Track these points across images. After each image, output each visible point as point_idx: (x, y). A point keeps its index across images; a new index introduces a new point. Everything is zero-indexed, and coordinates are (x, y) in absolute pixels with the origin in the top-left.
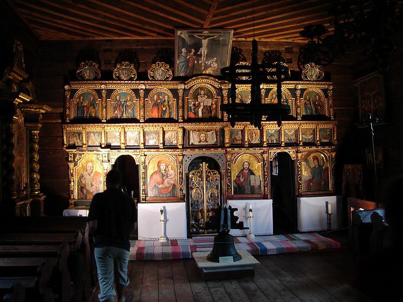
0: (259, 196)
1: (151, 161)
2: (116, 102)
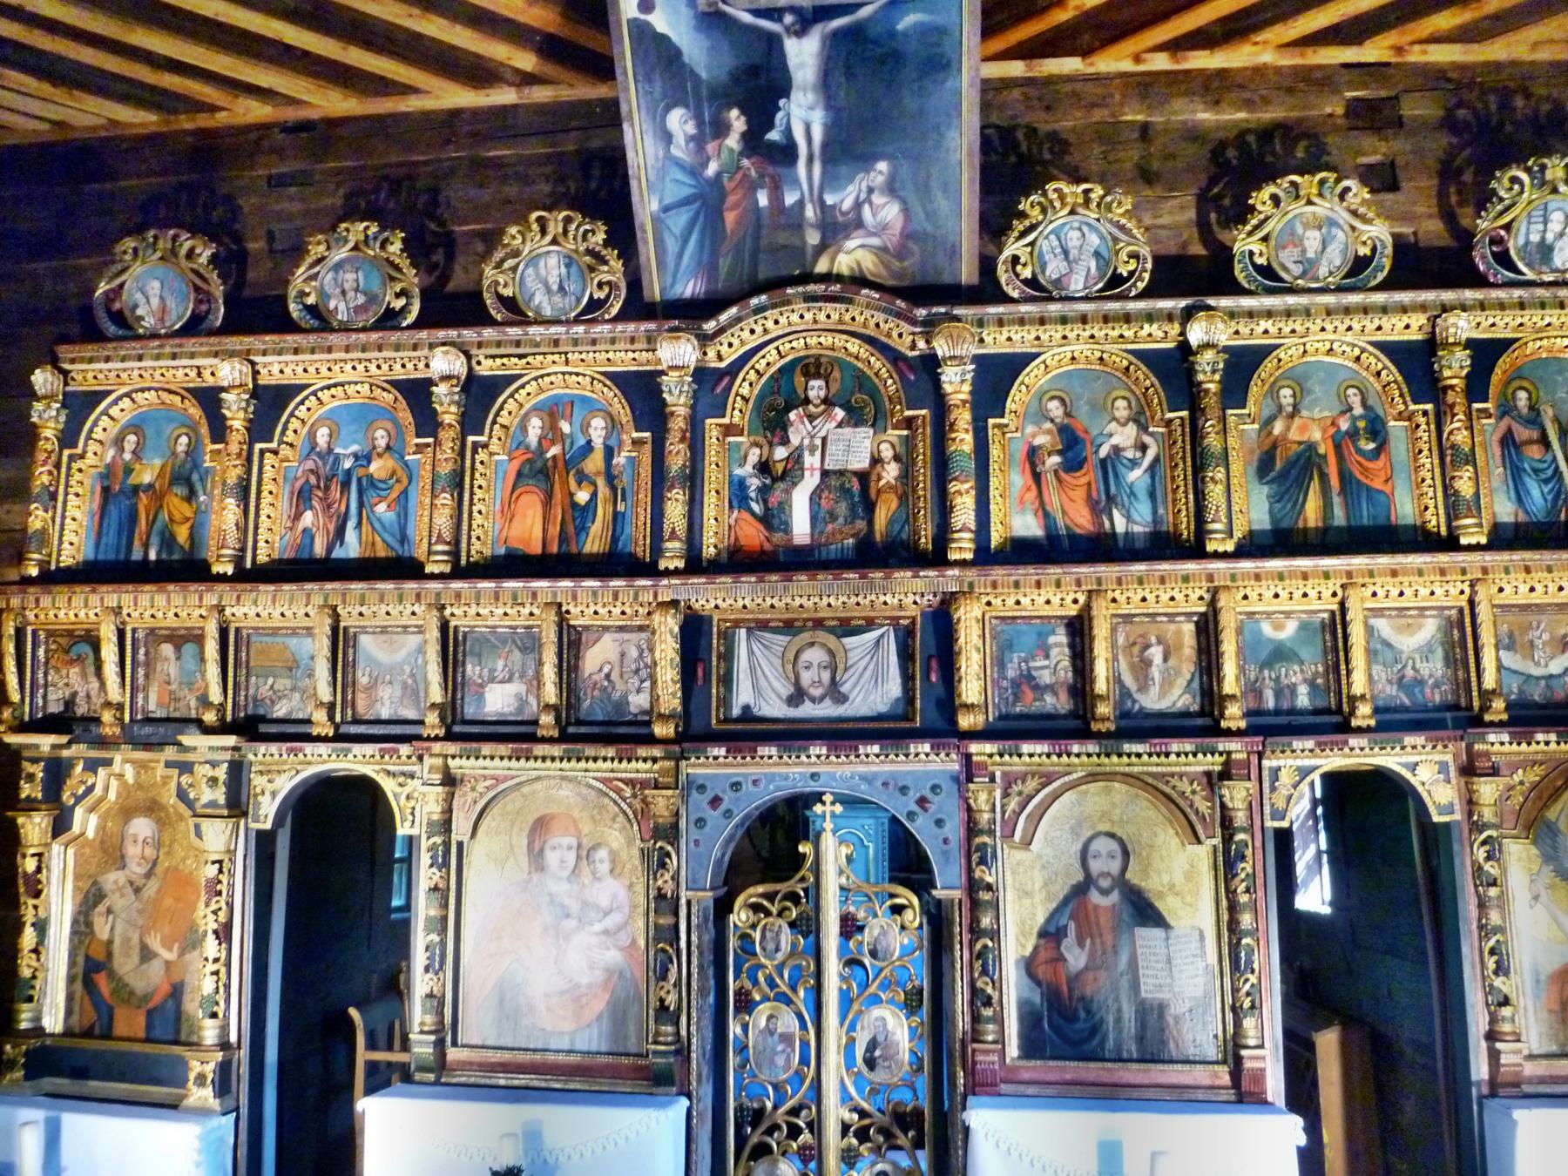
1: (495, 810)
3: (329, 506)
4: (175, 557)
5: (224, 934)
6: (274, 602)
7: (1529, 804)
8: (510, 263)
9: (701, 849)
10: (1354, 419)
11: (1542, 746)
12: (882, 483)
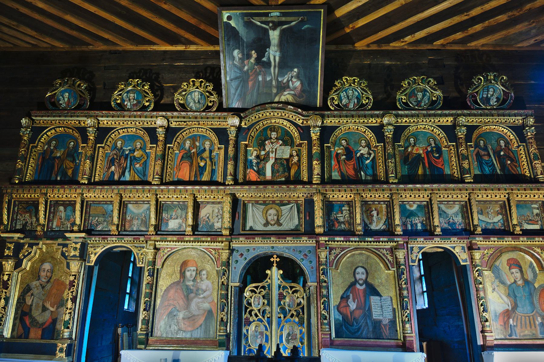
0: (393, 342)
1: (170, 259)
2: (114, 152)
3: (120, 165)
4: (67, 179)
5: (74, 300)
6: (101, 192)
7: (490, 260)
8: (184, 93)
9: (236, 270)
10: (432, 148)
11: (537, 243)
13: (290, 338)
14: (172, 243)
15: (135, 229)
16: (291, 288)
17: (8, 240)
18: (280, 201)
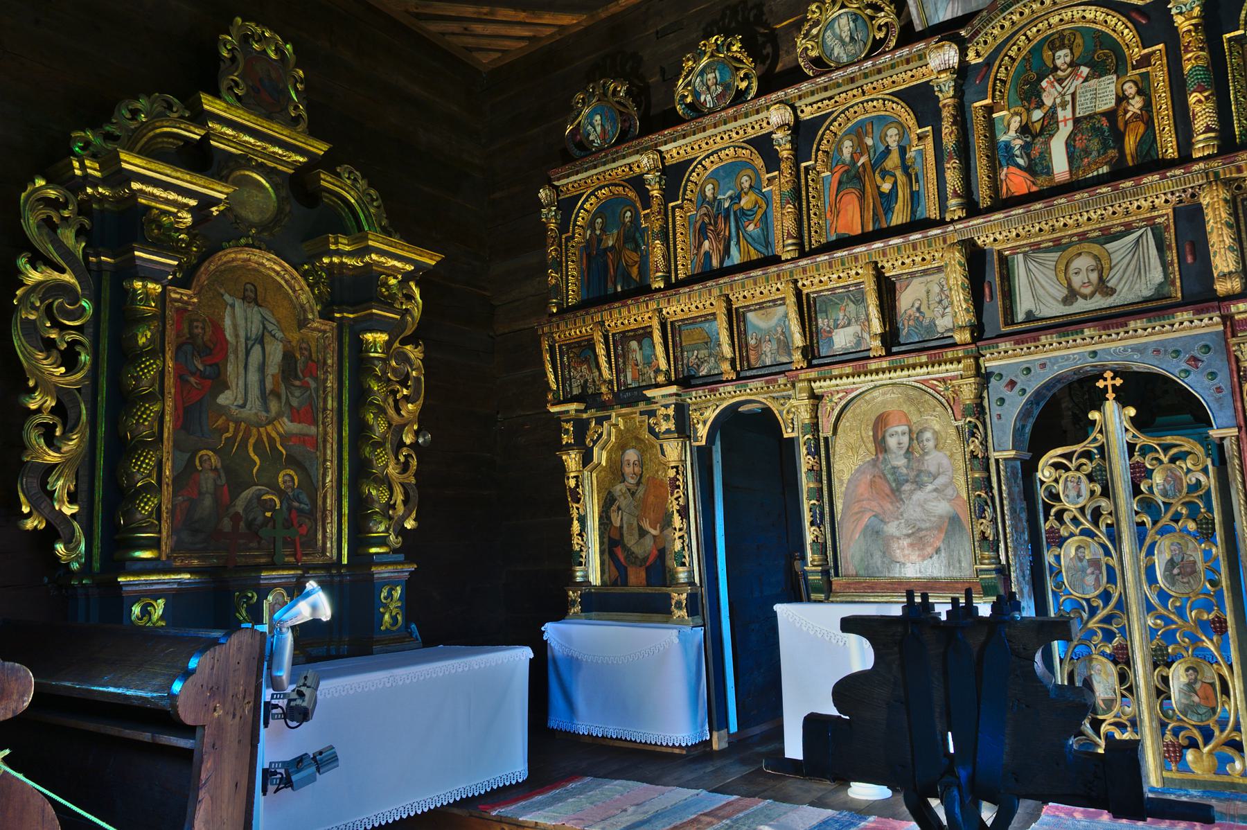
1: (848, 414)
5: (684, 512)
8: (814, 31)
9: (1002, 421)
12: (1128, 115)
13: (1176, 571)
14: (845, 380)
15: (768, 363)
16: (1166, 448)
17: (564, 417)
18: (1100, 229)
